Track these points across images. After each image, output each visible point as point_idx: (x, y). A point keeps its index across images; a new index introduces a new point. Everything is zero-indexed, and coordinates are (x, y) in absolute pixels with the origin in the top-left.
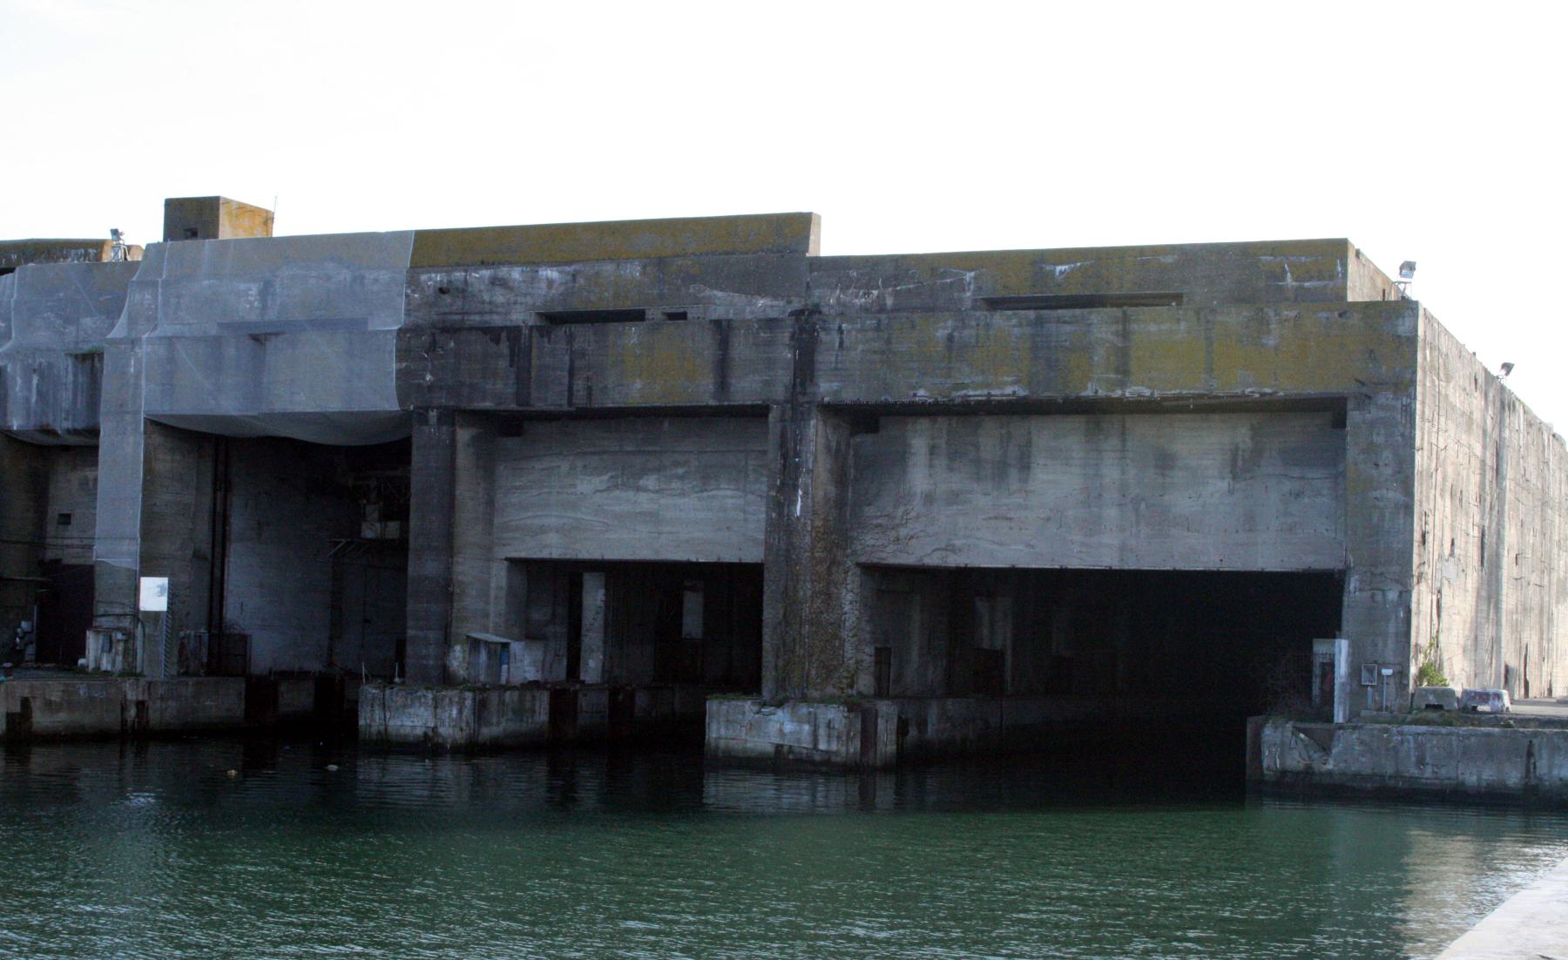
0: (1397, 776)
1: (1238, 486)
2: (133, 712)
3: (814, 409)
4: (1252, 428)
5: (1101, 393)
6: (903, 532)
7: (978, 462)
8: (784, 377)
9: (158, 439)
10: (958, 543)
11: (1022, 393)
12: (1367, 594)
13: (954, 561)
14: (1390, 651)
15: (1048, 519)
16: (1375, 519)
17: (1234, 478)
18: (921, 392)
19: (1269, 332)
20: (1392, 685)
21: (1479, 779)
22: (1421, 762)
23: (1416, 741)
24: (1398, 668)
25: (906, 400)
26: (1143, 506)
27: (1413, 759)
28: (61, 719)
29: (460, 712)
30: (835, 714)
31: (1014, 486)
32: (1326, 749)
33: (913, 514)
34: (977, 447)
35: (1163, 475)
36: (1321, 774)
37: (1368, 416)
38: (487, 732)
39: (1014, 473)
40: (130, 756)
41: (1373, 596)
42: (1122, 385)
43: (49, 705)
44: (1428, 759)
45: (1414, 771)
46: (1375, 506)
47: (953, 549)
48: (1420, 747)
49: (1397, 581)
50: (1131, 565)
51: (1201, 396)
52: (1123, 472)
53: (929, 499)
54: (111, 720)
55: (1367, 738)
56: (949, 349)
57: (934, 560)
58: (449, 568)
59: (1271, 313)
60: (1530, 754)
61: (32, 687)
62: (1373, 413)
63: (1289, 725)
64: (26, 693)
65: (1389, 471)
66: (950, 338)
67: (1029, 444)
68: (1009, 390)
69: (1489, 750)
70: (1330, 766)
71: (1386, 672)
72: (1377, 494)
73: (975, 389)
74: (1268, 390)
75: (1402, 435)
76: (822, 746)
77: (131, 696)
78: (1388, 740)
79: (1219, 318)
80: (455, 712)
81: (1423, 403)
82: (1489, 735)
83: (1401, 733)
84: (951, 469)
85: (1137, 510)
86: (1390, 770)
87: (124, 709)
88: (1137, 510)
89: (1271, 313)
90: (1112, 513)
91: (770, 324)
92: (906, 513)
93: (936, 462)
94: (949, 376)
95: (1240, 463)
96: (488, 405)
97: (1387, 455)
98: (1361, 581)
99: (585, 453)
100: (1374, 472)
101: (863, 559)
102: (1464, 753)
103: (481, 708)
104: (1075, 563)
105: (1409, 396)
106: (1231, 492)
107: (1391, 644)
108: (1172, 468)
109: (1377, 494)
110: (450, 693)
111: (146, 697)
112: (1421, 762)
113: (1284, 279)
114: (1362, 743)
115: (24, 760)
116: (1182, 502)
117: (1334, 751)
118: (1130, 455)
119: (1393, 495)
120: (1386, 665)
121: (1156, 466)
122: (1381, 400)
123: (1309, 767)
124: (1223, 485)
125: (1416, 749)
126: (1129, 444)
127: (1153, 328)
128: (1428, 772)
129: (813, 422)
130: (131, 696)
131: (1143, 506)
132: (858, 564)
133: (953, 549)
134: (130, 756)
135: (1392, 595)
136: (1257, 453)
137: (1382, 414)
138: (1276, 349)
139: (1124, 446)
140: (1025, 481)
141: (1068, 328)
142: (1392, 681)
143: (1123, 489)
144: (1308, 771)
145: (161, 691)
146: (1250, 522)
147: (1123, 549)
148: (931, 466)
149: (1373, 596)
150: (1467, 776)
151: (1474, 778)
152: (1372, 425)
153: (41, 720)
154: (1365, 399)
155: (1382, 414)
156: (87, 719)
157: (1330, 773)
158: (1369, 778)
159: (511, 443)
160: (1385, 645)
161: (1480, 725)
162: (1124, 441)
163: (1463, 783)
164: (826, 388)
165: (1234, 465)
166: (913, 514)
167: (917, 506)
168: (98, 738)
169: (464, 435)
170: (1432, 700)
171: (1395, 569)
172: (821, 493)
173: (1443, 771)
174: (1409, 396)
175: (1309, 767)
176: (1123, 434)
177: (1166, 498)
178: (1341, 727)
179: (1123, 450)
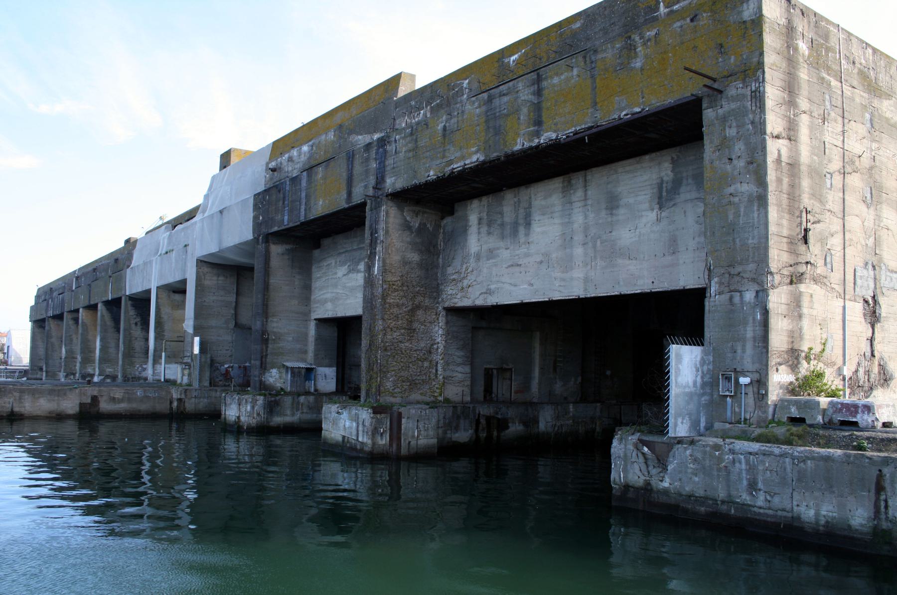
0: (729, 501)
1: (664, 214)
2: (175, 404)
3: (384, 198)
4: (673, 162)
5: (527, 145)
6: (466, 282)
7: (502, 225)
9: (206, 269)
10: (492, 287)
11: (482, 158)
12: (726, 297)
13: (492, 300)
14: (747, 357)
15: (541, 262)
16: (731, 217)
17: (660, 208)
18: (432, 173)
19: (636, 56)
20: (751, 395)
21: (817, 514)
22: (752, 486)
23: (748, 462)
24: (756, 376)
25: (423, 181)
26: (599, 243)
27: (745, 482)
28: (122, 407)
29: (253, 407)
30: (365, 415)
31: (522, 239)
32: (662, 463)
33: (470, 269)
34: (501, 213)
35: (611, 214)
36: (658, 491)
37: (721, 111)
38: (278, 420)
39: (522, 230)
40: (174, 425)
41: (731, 298)
42: (538, 134)
43: (113, 400)
44: (760, 485)
45: (745, 497)
46: (730, 203)
47: (489, 292)
48: (751, 469)
49: (753, 280)
50: (592, 294)
51: (591, 127)
52: (586, 217)
53: (478, 257)
54: (162, 407)
55: (699, 455)
56: (444, 136)
57: (479, 302)
58: (264, 325)
59: (637, 38)
60: (880, 488)
61: (100, 391)
62: (726, 107)
63: (635, 438)
64: (95, 393)
65: (741, 163)
66: (445, 128)
67: (530, 206)
68: (474, 158)
69: (827, 478)
70: (666, 484)
71: (744, 380)
72: (731, 189)
73: (457, 163)
74: (638, 110)
75: (753, 123)
76: (360, 439)
77: (176, 395)
78: (720, 459)
79: (600, 56)
80: (249, 408)
81: (791, 88)
82: (827, 459)
83: (732, 452)
84: (489, 233)
85: (594, 247)
86: (722, 494)
87: (171, 403)
88: (594, 247)
89: (637, 38)
90: (579, 251)
91: (368, 146)
92: (467, 269)
93: (482, 230)
94: (444, 157)
95: (664, 194)
96: (276, 229)
97: (739, 147)
98: (720, 283)
99: (340, 253)
100: (729, 167)
101: (446, 305)
102: (799, 480)
103: (272, 407)
104: (557, 296)
105: (757, 80)
106: (659, 220)
107: (749, 350)
108: (618, 207)
109: (731, 189)
110: (246, 396)
111: (183, 396)
112: (752, 486)
113: (657, 9)
114: (695, 460)
115: (94, 431)
116: (625, 236)
117: (669, 468)
118: (589, 202)
119: (747, 188)
120: (744, 373)
121: (606, 209)
122: (732, 92)
123: (648, 483)
124: (652, 216)
125: (748, 471)
126: (589, 193)
127: (556, 80)
129: (383, 208)
130: (176, 395)
131: (599, 243)
132: (444, 308)
133: (489, 292)
134: (174, 425)
135: (749, 296)
136: (677, 184)
137: (733, 106)
138: (642, 69)
139: (586, 195)
140: (527, 235)
141: (505, 99)
142: (750, 390)
143: (586, 228)
144: (647, 488)
145: (194, 394)
146: (673, 245)
147: (586, 280)
148: (479, 233)
149: (731, 298)
150: (802, 509)
151: (812, 513)
152: (724, 119)
153: (105, 406)
154: (717, 93)
155: (733, 106)
156: (144, 407)
157: (666, 492)
158: (702, 500)
159: (316, 253)
160: (744, 351)
161: (827, 445)
162: (586, 191)
163: (799, 518)
164: (392, 183)
165: (660, 197)
166: (470, 269)
167: (472, 263)
168: (153, 417)
169: (276, 250)
170: (794, 412)
171: (752, 266)
172: (395, 258)
173: (776, 500)
174: (757, 80)
175: (648, 483)
176: (585, 186)
177: (614, 233)
178: (680, 441)
179: (586, 199)
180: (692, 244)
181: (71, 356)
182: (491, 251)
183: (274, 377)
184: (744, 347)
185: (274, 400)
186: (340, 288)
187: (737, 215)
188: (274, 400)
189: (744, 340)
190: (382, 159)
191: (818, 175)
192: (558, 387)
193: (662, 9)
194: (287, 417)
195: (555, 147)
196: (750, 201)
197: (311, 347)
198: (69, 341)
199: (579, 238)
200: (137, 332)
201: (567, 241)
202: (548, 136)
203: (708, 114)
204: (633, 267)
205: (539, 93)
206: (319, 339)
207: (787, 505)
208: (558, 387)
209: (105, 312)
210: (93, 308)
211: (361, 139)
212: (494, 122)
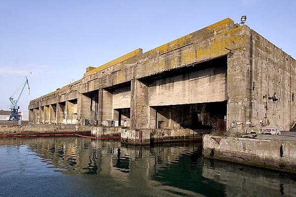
4: (214, 71)
8: (132, 75)
16: (235, 84)
22: (244, 148)
23: (243, 143)
62: (234, 57)
91: (131, 67)
103: (104, 130)
106: (209, 85)
112: (244, 148)
116: (200, 89)
127: (185, 51)
128: (247, 151)
146: (213, 91)
154: (231, 54)
164: (139, 76)
180: (219, 91)
181: (41, 118)
182: (163, 93)
183: (105, 123)
184: (238, 116)
185: (104, 128)
186: (122, 101)
187: (237, 84)
188: (104, 128)
189: (238, 114)
190: (135, 71)
191: (257, 75)
192: (175, 125)
193: (215, 33)
194: (109, 132)
195: (185, 68)
196: (241, 80)
197: (113, 116)
198: (41, 114)
199: (187, 89)
200: (61, 112)
201: (184, 90)
202: (183, 65)
203: (229, 59)
204: (201, 96)
205: (180, 54)
206: (114, 113)
207: (254, 153)
208: (175, 125)
209: (52, 108)
210: (48, 106)
211: (129, 65)
212: (167, 62)
